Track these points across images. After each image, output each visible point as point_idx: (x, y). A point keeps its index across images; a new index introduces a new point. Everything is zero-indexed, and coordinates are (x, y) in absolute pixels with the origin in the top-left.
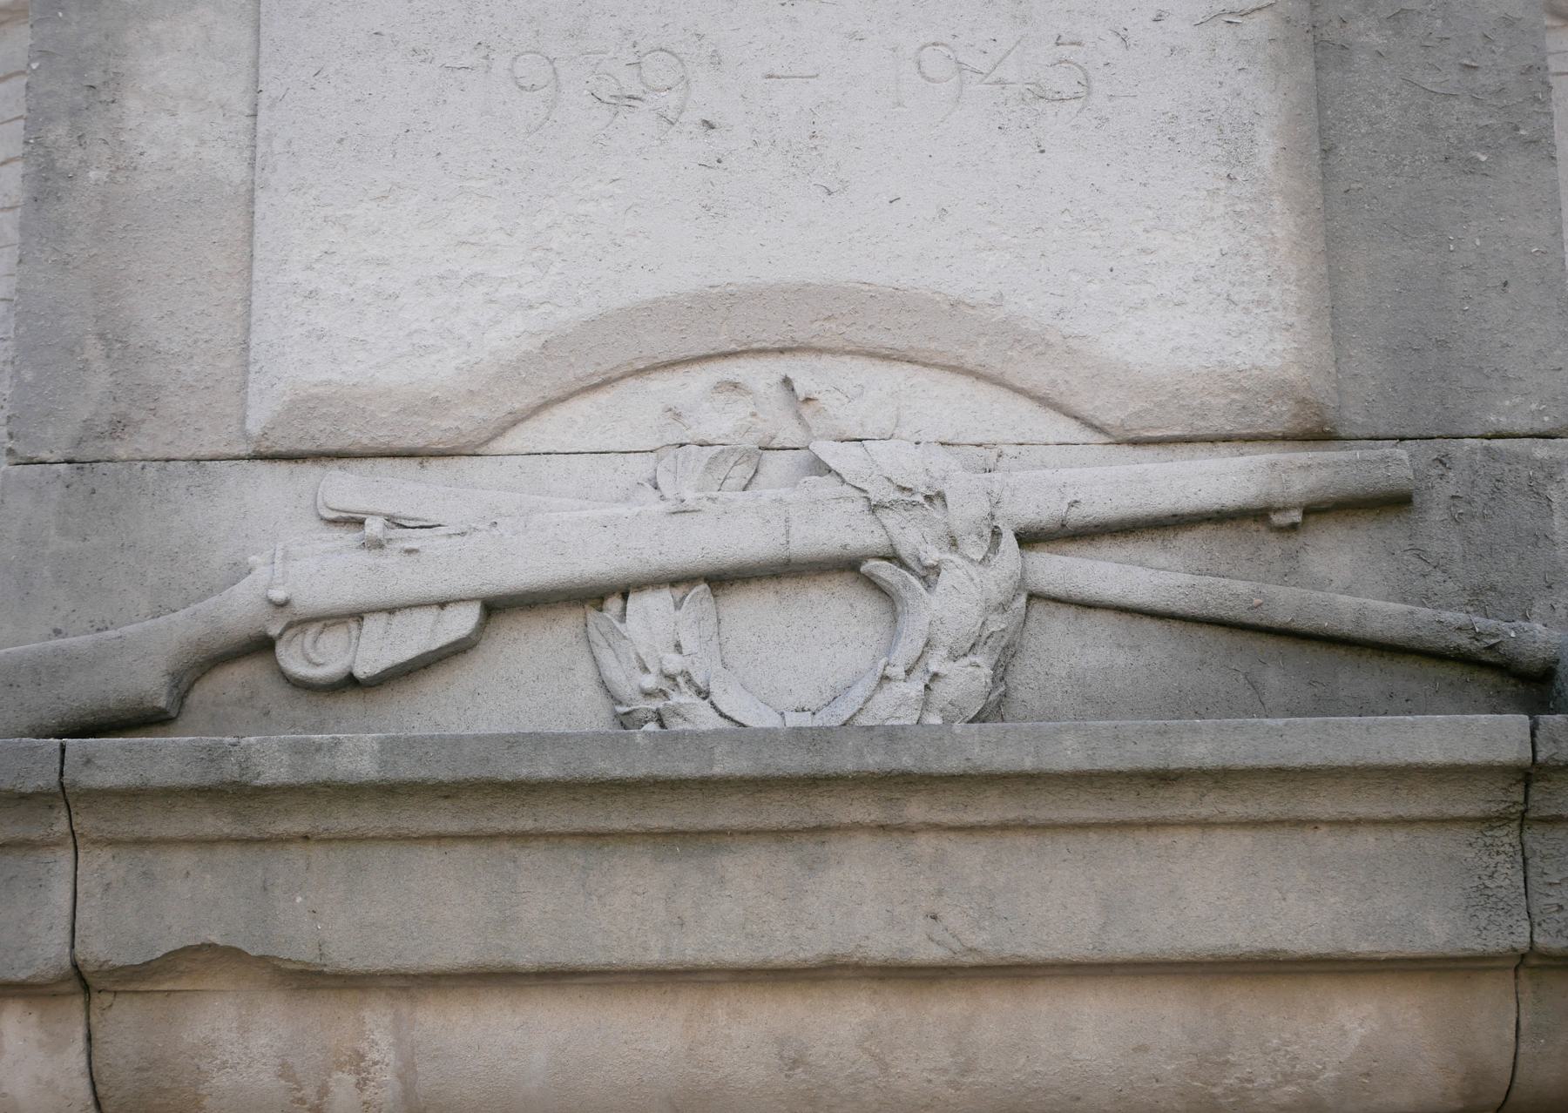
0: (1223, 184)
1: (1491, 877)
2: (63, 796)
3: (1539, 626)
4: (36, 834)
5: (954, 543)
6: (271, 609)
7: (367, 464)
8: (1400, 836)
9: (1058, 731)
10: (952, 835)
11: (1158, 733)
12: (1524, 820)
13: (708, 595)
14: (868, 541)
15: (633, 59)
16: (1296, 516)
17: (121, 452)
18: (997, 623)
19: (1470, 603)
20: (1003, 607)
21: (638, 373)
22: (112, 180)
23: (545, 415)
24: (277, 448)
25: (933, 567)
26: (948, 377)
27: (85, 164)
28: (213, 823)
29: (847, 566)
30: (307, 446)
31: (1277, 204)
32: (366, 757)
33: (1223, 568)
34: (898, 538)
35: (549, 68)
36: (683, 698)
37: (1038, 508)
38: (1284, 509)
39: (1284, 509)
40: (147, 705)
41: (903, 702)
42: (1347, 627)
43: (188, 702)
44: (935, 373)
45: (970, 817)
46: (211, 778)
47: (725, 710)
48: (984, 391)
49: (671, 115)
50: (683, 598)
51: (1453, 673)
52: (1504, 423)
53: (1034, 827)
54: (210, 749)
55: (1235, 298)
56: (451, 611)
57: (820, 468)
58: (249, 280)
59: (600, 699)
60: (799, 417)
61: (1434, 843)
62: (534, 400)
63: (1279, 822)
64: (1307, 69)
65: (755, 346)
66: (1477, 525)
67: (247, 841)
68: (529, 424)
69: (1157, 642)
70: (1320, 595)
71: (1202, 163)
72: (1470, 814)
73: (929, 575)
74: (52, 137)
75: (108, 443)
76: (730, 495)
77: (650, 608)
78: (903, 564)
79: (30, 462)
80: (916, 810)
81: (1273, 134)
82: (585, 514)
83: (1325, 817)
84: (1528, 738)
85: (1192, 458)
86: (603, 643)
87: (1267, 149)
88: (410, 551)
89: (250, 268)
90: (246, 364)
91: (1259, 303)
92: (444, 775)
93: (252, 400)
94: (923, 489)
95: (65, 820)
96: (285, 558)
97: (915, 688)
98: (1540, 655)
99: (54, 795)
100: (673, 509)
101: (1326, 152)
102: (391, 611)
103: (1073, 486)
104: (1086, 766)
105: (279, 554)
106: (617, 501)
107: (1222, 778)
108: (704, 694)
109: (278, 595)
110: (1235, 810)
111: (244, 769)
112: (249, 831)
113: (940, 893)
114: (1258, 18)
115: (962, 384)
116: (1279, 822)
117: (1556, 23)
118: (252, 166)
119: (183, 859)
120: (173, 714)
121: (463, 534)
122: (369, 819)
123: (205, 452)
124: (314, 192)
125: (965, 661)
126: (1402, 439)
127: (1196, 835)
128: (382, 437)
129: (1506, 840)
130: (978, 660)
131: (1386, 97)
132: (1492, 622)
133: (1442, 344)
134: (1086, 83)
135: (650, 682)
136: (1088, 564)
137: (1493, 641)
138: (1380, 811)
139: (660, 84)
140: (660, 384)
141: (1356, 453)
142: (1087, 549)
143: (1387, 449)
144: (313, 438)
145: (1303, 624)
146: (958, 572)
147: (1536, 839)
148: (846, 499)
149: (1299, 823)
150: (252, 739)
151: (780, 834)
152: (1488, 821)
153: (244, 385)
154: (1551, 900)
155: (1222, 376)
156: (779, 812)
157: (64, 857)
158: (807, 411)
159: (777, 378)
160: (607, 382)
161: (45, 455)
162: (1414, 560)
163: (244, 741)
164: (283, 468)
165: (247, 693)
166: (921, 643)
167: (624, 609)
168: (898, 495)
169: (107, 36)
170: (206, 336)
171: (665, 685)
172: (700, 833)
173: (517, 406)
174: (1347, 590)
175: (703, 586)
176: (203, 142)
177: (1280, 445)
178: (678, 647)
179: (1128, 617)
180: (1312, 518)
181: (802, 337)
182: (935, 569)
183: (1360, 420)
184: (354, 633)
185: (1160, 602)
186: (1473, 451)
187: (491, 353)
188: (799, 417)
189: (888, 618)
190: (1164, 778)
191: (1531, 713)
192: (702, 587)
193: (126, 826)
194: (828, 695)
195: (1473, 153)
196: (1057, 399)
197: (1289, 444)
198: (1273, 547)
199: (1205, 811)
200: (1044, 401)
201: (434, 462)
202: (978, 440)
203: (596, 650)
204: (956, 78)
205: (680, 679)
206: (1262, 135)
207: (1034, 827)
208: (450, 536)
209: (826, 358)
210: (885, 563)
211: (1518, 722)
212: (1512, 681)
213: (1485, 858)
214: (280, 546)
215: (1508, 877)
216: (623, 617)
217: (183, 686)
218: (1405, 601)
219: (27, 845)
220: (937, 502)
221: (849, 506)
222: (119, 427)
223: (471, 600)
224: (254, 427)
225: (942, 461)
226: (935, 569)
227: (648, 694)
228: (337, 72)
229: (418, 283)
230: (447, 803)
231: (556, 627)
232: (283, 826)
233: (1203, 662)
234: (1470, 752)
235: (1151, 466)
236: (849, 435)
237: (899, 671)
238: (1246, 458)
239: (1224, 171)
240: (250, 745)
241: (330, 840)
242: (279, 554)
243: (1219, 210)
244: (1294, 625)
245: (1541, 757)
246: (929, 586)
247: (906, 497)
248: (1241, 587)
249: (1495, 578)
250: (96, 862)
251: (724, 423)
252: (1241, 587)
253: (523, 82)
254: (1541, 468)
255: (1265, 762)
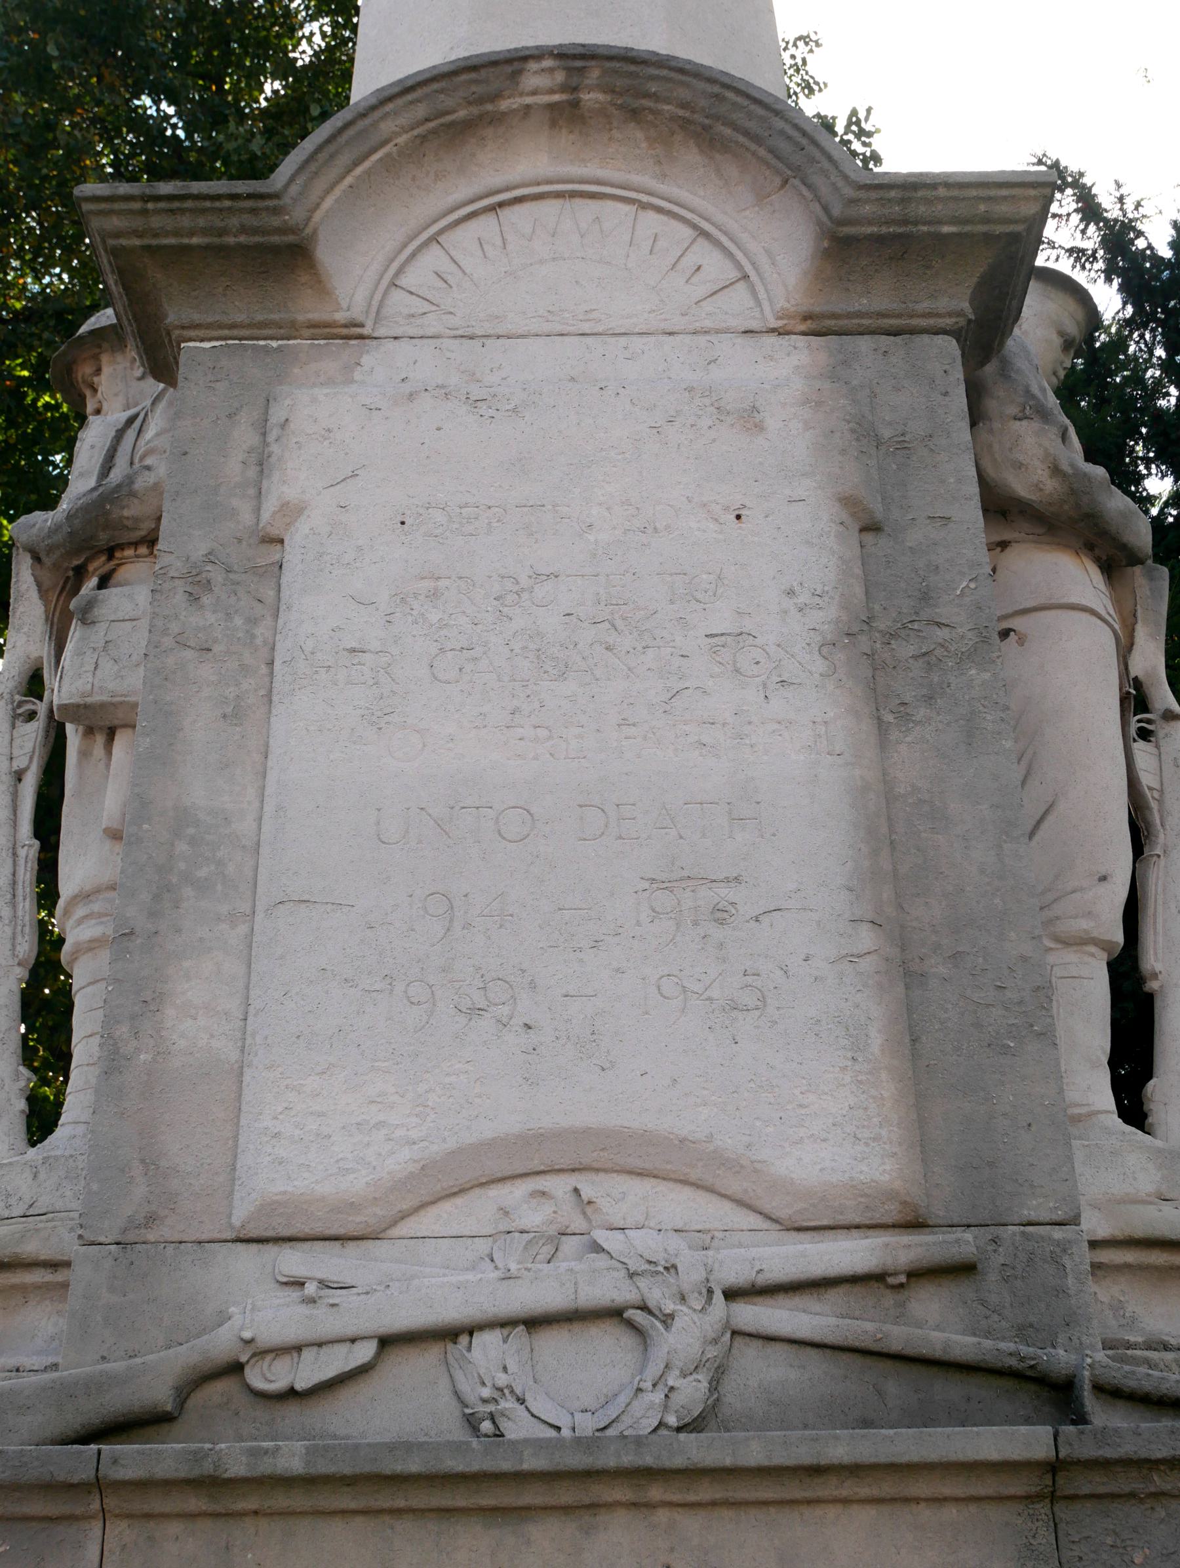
0: (850, 1063)
1: (1034, 1537)
2: (98, 1485)
3: (1061, 1352)
4: (79, 1511)
5: (683, 1299)
6: (242, 1344)
7: (307, 1245)
8: (973, 1508)
9: (747, 1439)
10: (680, 1510)
11: (812, 1439)
12: (1053, 1498)
13: (525, 1333)
14: (628, 1298)
15: (482, 985)
16: (902, 1279)
17: (151, 1237)
18: (712, 1352)
19: (1017, 1336)
20: (715, 1341)
21: (482, 1185)
22: (154, 1060)
23: (422, 1213)
24: (251, 1235)
25: (669, 1315)
26: (679, 1186)
27: (138, 1050)
28: (195, 1503)
29: (615, 1314)
30: (270, 1234)
31: (884, 1075)
32: (297, 1458)
33: (857, 1313)
34: (647, 1295)
35: (429, 991)
36: (508, 1404)
37: (736, 1273)
38: (895, 1274)
39: (895, 1274)
40: (159, 1409)
41: (651, 1406)
42: (938, 1354)
43: (186, 1406)
44: (671, 1185)
45: (692, 1497)
46: (196, 1473)
47: (535, 1413)
48: (702, 1197)
49: (505, 1020)
50: (508, 1336)
51: (1009, 1384)
52: (1033, 1216)
53: (733, 1504)
54: (195, 1453)
55: (860, 1136)
56: (358, 1344)
57: (597, 1248)
58: (237, 1124)
59: (454, 1402)
60: (584, 1213)
61: (996, 1514)
62: (416, 1203)
63: (893, 1500)
64: (900, 989)
65: (556, 1167)
66: (1018, 1283)
67: (216, 1515)
68: (412, 1218)
69: (817, 1365)
70: (920, 1331)
71: (837, 1050)
72: (1019, 1493)
73: (667, 1320)
74: (118, 1033)
75: (143, 1231)
76: (540, 1266)
77: (488, 1341)
78: (650, 1312)
79: (92, 1244)
80: (656, 1493)
81: (879, 1031)
82: (446, 1279)
83: (923, 1496)
84: (1052, 1443)
85: (835, 1240)
86: (456, 1366)
87: (876, 1041)
88: (333, 1305)
89: (238, 1117)
90: (234, 1180)
91: (874, 1139)
92: (347, 1470)
93: (236, 1203)
94: (663, 1263)
95: (98, 1502)
96: (253, 1309)
97: (658, 1397)
98: (1063, 1372)
99: (91, 1484)
100: (503, 1276)
101: (914, 1041)
102: (320, 1345)
103: (759, 1259)
104: (766, 1463)
105: (249, 1307)
106: (467, 1269)
107: (855, 1470)
108: (521, 1401)
109: (247, 1335)
110: (865, 1491)
111: (216, 1467)
112: (218, 1508)
113: (672, 1550)
114: (868, 958)
115: (687, 1192)
116: (893, 1500)
117: (1059, 946)
118: (242, 1051)
119: (175, 1527)
120: (176, 1415)
121: (367, 1293)
122: (298, 1500)
123: (204, 1237)
124: (280, 1069)
125: (691, 1378)
126: (969, 1226)
127: (839, 1508)
128: (319, 1228)
129: (1042, 1511)
130: (700, 1377)
131: (950, 1006)
132: (1031, 1349)
133: (991, 1165)
134: (763, 999)
135: (486, 1392)
136: (769, 1311)
137: (1033, 1363)
138: (959, 1492)
139: (497, 1001)
140: (494, 1192)
141: (938, 1237)
142: (769, 1301)
143: (959, 1233)
144: (274, 1228)
145: (909, 1351)
146: (686, 1318)
147: (1063, 1511)
148: (614, 1269)
149: (907, 1500)
150: (223, 1446)
151: (567, 1510)
152: (1029, 1498)
153: (231, 1193)
154: (1076, 1554)
155: (852, 1186)
156: (566, 1495)
157: (97, 1526)
158: (589, 1210)
159: (569, 1188)
160: (462, 1191)
161: (102, 1239)
162: (980, 1307)
163: (218, 1447)
164: (254, 1247)
165: (225, 1400)
166: (662, 1366)
167: (471, 1342)
168: (647, 1267)
169: (156, 970)
170: (209, 1161)
171: (496, 1395)
172: (515, 1509)
173: (404, 1207)
174: (937, 1328)
175: (522, 1327)
176: (212, 1036)
177: (891, 1231)
178: (505, 1369)
179: (796, 1346)
180: (913, 1279)
181: (586, 1161)
182: (671, 1316)
183: (941, 1213)
184: (296, 1360)
185: (817, 1337)
186: (1014, 1234)
187: (389, 1173)
188: (584, 1213)
189: (641, 1348)
190: (816, 1471)
191: (1056, 1423)
192: (521, 1328)
193: (138, 1505)
194: (602, 1400)
195: (1005, 1042)
196: (749, 1202)
197: (897, 1230)
198: (889, 1299)
199: (844, 1493)
200: (740, 1203)
201: (351, 1244)
202: (699, 1227)
203: (452, 1370)
204: (682, 997)
205: (506, 1391)
206: (873, 1033)
207: (733, 1504)
208: (359, 1294)
209: (602, 1175)
210: (639, 1311)
211: (1044, 1432)
212: (1047, 1389)
213: (1029, 1524)
214: (250, 1301)
215: (1045, 1537)
216: (469, 1349)
217: (183, 1395)
218: (974, 1335)
219: (72, 1518)
220: (672, 1271)
221: (615, 1274)
222: (151, 1220)
223: (372, 1337)
224: (236, 1221)
225: (676, 1243)
226: (671, 1316)
227: (485, 1401)
228: (297, 993)
229: (344, 1128)
230: (346, 1489)
231: (426, 1355)
232: (241, 1505)
233: (846, 1377)
234: (1015, 1453)
235: (808, 1246)
236: (615, 1225)
237: (648, 1385)
238: (869, 1240)
239: (849, 1055)
240: (221, 1450)
241: (271, 1514)
242: (249, 1307)
243: (848, 1079)
244: (904, 1352)
245: (1061, 1455)
246: (667, 1327)
247: (652, 1268)
248: (869, 1326)
249: (1032, 1319)
250: (119, 1530)
251: (534, 1217)
252: (869, 1326)
253: (412, 1000)
254: (1058, 1245)
255: (883, 1459)
